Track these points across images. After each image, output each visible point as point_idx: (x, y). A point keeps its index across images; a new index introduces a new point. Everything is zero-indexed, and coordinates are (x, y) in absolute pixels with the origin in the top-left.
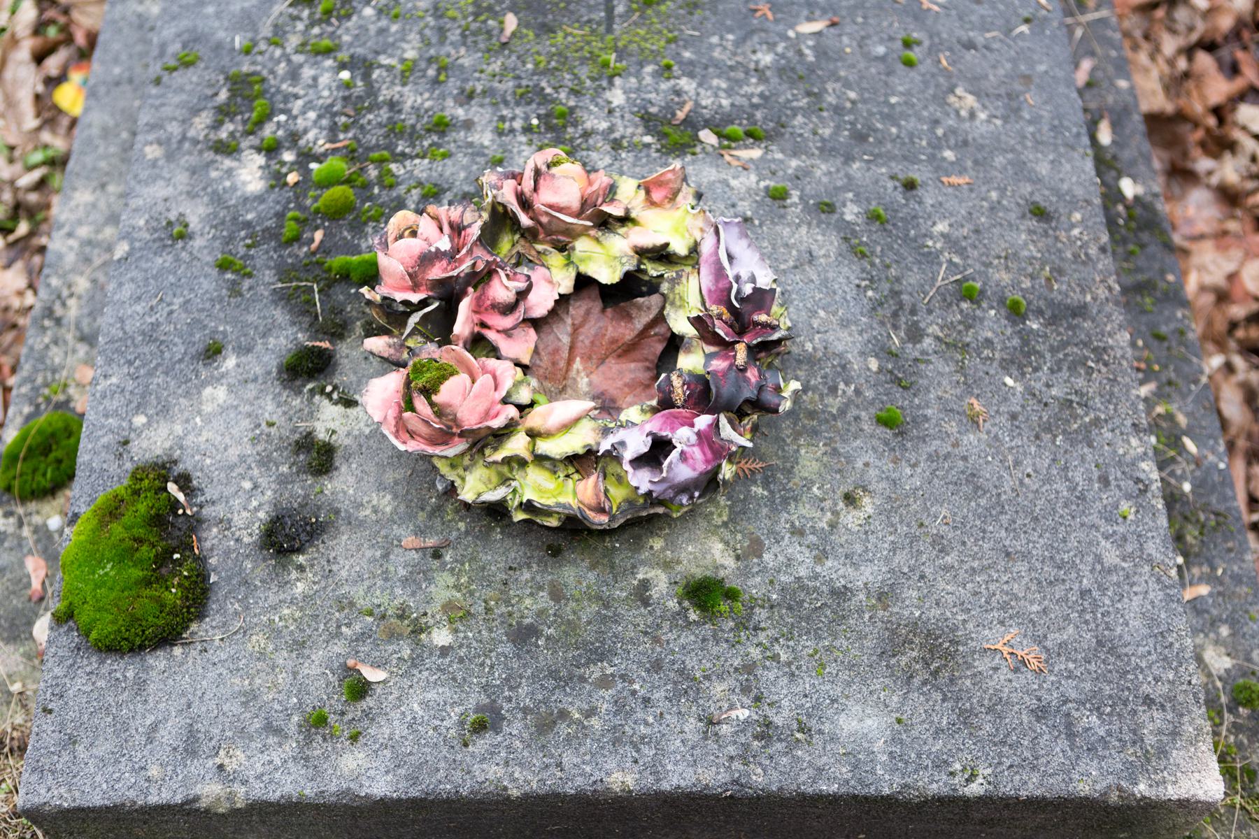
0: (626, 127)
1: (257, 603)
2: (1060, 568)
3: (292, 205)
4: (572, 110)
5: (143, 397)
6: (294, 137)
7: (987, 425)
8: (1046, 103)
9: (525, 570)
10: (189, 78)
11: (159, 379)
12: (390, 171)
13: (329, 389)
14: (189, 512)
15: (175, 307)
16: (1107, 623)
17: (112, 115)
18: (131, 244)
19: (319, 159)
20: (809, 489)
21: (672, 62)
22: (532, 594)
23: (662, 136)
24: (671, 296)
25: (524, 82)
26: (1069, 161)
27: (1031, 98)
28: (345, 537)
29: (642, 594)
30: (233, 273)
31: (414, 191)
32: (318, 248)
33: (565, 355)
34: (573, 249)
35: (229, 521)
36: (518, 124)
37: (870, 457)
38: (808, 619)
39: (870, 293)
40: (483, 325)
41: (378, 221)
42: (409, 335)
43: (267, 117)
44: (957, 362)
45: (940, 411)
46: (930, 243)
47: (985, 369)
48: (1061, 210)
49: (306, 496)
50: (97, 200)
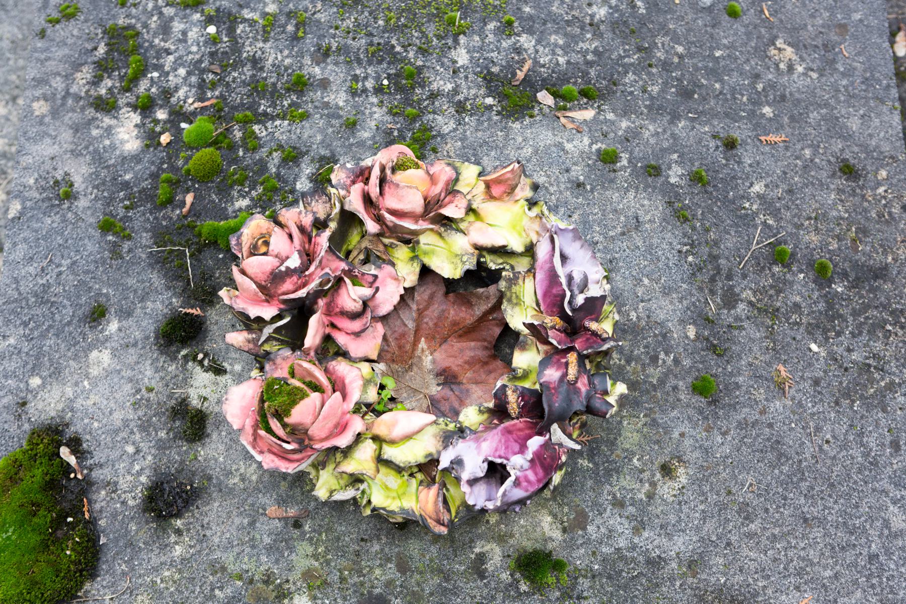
0: (469, 88)
1: (140, 564)
2: (852, 533)
3: (165, 166)
4: (420, 70)
5: (37, 359)
6: (167, 94)
7: (793, 391)
8: (859, 54)
9: (375, 542)
10: (70, 31)
11: (50, 342)
12: (253, 132)
13: (200, 356)
14: (79, 476)
15: (63, 269)
16: (891, 587)
17: (19, 28)
18: (23, 203)
19: (189, 118)
20: (630, 460)
21: (513, 18)
22: (381, 565)
23: (502, 97)
24: (508, 294)
25: (376, 40)
26: (878, 115)
27: (846, 49)
28: (216, 504)
29: (478, 567)
30: (113, 235)
31: (275, 154)
32: (190, 211)
33: (411, 338)
34: (418, 242)
35: (116, 483)
36: (370, 84)
37: (685, 427)
38: (625, 587)
39: (690, 259)
40: (333, 326)
41: (242, 185)
42: (267, 340)
43: (141, 73)
44: (768, 327)
45: (750, 378)
46: (747, 205)
47: (792, 333)
48: (869, 168)
49: (182, 462)
50: (10, 113)
